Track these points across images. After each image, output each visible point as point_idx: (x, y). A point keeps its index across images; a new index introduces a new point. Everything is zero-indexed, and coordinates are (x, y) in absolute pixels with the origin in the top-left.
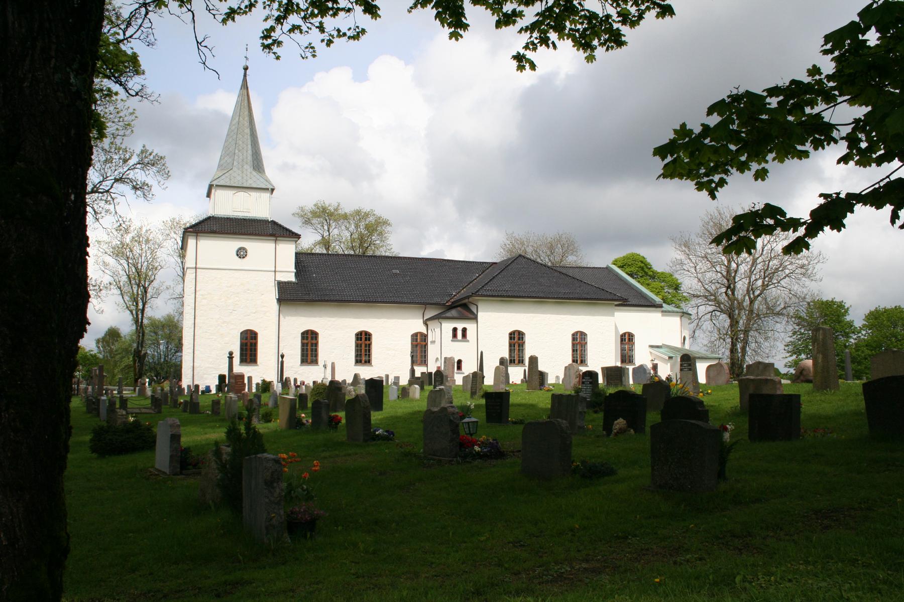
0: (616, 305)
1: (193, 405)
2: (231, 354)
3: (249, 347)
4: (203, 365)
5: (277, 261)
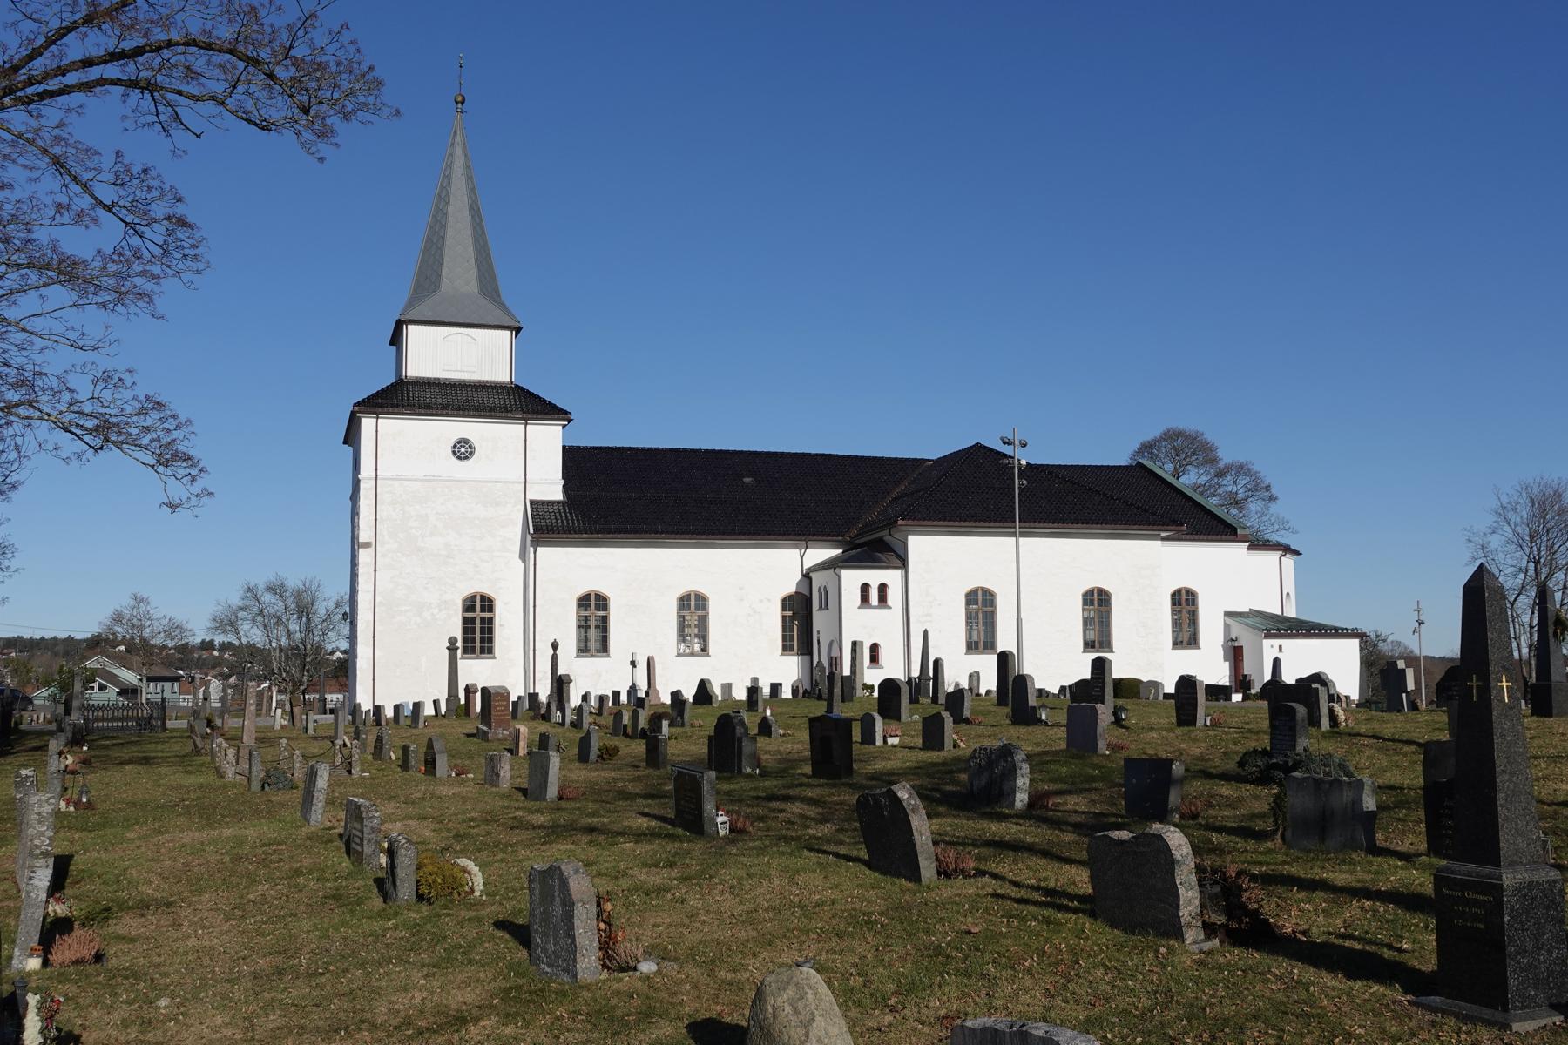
0: (1164, 539)
1: (405, 744)
2: (452, 641)
3: (478, 629)
4: (400, 668)
5: (533, 459)
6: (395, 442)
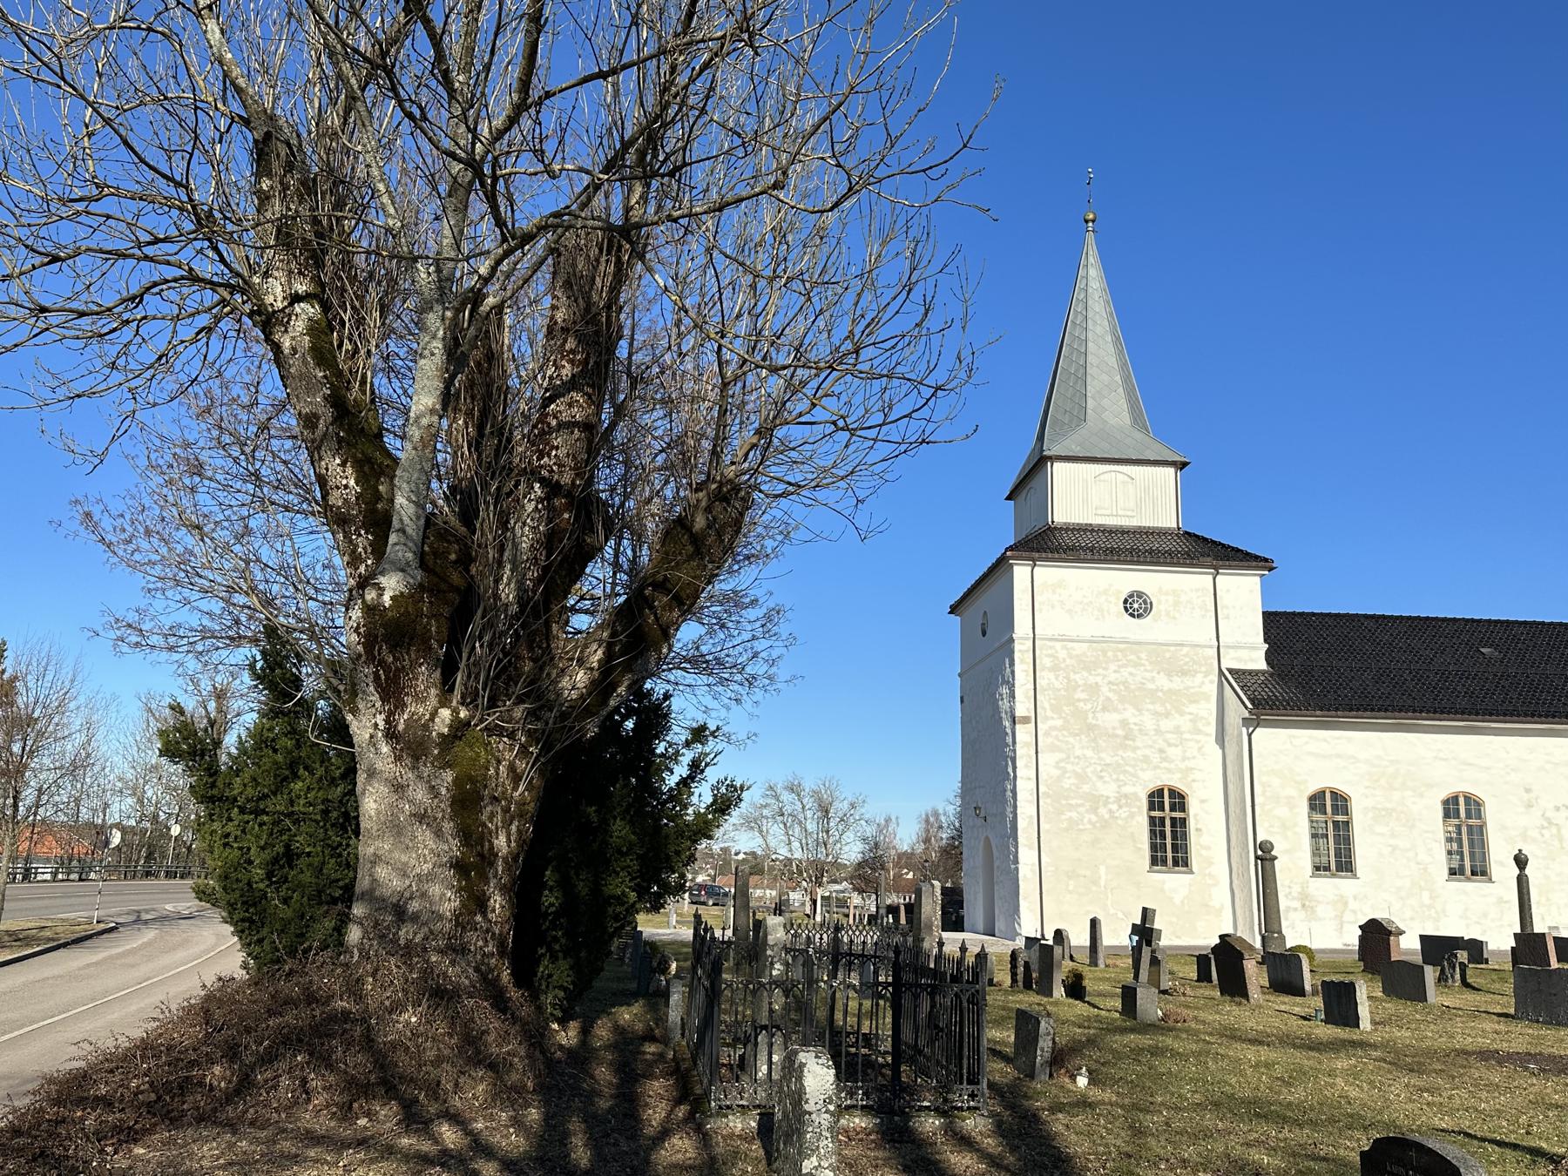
3: (1169, 840)
5: (1225, 618)
6: (1051, 598)
